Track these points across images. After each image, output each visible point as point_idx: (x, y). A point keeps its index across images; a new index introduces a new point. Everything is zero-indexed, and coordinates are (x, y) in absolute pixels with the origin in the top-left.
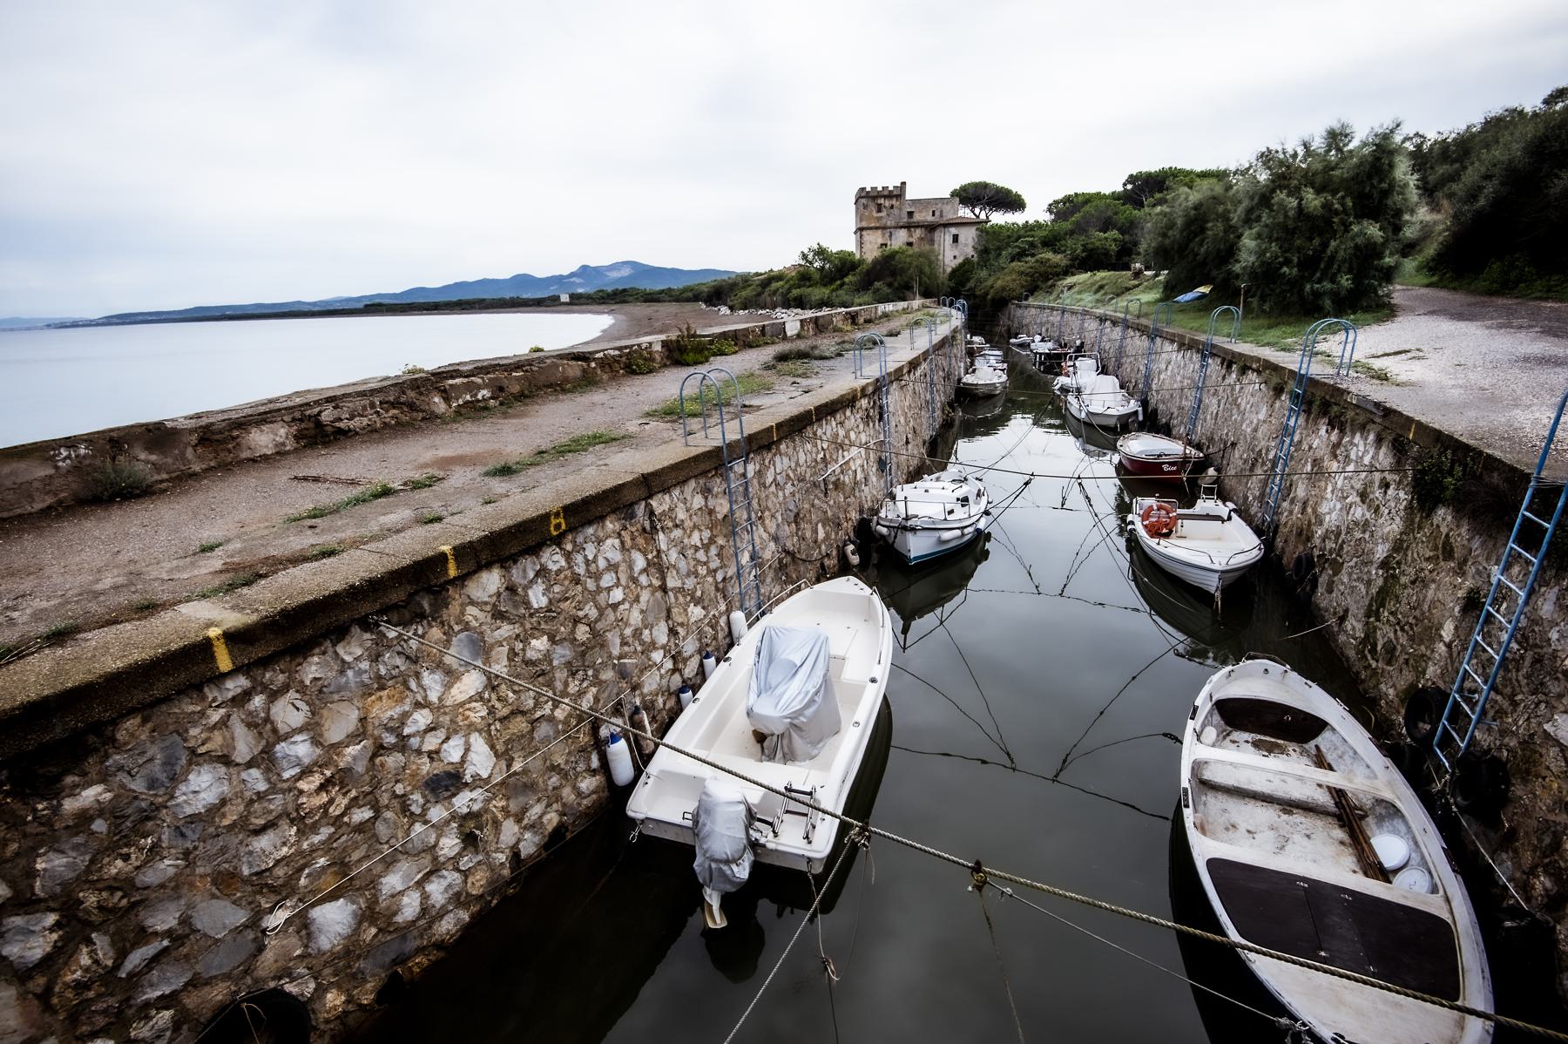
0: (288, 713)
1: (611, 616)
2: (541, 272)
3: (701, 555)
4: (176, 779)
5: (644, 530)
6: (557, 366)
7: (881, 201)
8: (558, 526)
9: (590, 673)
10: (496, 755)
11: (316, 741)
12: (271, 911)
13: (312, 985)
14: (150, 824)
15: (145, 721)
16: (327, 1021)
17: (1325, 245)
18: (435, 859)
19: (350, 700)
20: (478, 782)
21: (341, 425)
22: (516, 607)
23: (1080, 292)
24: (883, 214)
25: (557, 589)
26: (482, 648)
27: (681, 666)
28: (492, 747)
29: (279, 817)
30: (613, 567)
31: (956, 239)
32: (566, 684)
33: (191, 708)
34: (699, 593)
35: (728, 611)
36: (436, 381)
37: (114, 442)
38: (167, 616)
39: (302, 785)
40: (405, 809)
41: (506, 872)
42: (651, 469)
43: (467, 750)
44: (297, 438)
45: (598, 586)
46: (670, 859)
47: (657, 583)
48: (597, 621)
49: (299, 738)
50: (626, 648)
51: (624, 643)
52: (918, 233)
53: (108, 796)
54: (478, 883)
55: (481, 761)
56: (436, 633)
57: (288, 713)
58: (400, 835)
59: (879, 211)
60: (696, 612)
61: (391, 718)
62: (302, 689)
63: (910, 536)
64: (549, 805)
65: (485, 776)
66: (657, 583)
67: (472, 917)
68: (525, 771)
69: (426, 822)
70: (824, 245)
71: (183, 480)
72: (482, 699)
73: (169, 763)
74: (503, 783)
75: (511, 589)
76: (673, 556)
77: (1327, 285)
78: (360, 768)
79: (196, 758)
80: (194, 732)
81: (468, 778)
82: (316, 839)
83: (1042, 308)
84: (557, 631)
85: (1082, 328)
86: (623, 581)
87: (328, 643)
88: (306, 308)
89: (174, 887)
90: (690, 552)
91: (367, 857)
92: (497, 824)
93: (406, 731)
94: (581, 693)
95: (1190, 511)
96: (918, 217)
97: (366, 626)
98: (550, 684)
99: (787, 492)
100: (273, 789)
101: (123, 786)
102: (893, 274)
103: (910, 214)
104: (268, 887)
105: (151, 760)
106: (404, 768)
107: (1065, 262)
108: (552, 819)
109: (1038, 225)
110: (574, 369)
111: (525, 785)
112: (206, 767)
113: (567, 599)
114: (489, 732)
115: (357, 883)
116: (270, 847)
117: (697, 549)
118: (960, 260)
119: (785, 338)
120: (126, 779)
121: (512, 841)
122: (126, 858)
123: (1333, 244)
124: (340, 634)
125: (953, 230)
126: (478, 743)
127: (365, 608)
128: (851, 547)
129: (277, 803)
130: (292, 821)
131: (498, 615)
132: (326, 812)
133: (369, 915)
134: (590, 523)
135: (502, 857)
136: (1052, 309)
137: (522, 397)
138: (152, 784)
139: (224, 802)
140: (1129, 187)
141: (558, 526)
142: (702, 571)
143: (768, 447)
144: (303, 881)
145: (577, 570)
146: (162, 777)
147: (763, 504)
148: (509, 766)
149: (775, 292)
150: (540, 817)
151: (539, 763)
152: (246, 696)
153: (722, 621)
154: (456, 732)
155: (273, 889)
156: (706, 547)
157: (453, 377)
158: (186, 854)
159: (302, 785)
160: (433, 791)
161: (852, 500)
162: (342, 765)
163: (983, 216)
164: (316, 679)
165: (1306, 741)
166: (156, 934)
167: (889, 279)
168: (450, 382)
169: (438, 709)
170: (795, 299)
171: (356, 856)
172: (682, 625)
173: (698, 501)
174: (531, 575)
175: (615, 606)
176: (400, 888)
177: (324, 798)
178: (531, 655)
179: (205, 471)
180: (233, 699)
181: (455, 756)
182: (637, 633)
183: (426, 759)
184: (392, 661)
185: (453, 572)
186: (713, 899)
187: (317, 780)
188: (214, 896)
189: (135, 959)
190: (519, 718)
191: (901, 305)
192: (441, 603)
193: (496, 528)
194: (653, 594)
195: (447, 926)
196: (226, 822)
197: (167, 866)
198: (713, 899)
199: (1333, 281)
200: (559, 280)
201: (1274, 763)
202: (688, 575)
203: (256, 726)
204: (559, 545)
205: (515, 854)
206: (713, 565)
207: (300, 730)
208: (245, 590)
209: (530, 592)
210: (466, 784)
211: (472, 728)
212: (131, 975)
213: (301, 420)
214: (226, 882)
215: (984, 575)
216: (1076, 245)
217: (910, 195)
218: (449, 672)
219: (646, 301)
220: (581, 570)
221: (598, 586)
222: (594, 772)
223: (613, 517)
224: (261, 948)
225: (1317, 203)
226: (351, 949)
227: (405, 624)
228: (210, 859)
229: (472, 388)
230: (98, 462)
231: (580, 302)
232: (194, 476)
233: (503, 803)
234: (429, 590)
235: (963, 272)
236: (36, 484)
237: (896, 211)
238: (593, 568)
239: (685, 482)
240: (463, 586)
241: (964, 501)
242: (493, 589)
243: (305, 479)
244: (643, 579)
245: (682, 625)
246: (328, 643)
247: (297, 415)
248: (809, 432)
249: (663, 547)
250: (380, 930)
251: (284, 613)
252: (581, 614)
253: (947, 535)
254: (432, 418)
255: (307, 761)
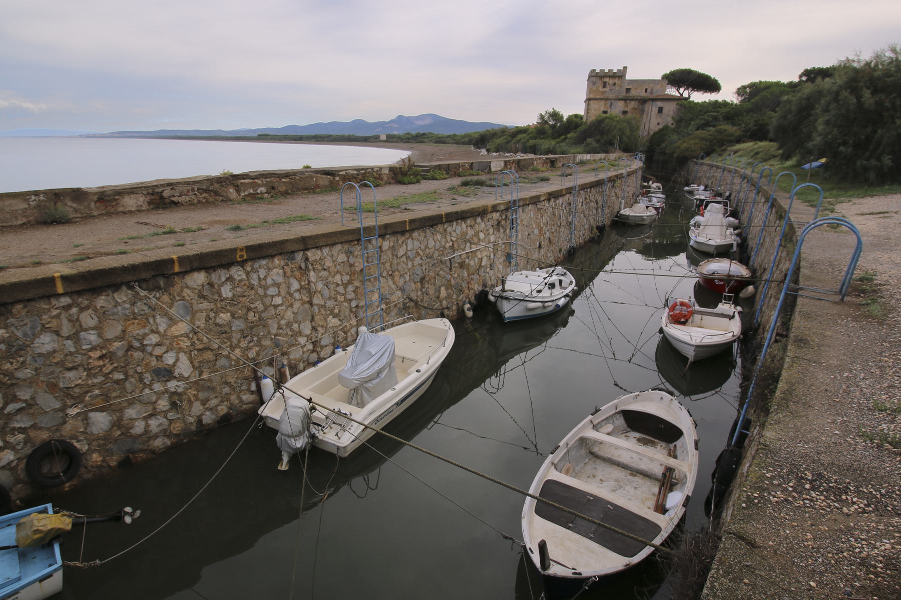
0: (88, 319)
1: (272, 311)
2: (371, 119)
3: (341, 289)
4: (36, 336)
5: (300, 268)
6: (312, 177)
7: (607, 80)
8: (241, 256)
9: (255, 339)
10: (193, 366)
11: (100, 335)
12: (71, 406)
13: (86, 447)
14: (22, 352)
15: (25, 307)
16: (92, 467)
17: (875, 132)
18: (155, 409)
19: (118, 320)
20: (181, 378)
21: (174, 199)
22: (213, 294)
23: (741, 156)
24: (607, 89)
25: (239, 289)
26: (192, 313)
27: (319, 349)
28: (191, 362)
29: (79, 365)
30: (278, 285)
31: (660, 110)
32: (239, 341)
33: (45, 306)
34: (336, 311)
35: (358, 326)
36: (232, 180)
37: (57, 195)
38: (43, 267)
39: (91, 354)
40: (141, 380)
41: (193, 428)
42: (308, 234)
43: (177, 360)
44: (149, 203)
45: (265, 293)
46: (267, 433)
47: (306, 299)
48: (262, 312)
49: (92, 332)
50: (281, 331)
51: (279, 328)
52: (633, 104)
53: (7, 335)
54: (177, 428)
55: (184, 367)
56: (166, 298)
57: (88, 319)
58: (137, 391)
59: (604, 86)
60: (333, 322)
61: (138, 334)
62: (96, 310)
63: (505, 302)
64: (222, 401)
65: (186, 376)
66: (306, 299)
67: (172, 444)
68: (209, 380)
69: (151, 389)
70: (557, 110)
71: (88, 217)
72: (188, 337)
73: (33, 328)
74: (196, 382)
75: (211, 285)
76: (320, 286)
77: (874, 162)
78: (120, 353)
79: (45, 329)
80: (44, 317)
81: (176, 374)
82: (95, 381)
83: (711, 166)
84: (237, 312)
85: (732, 183)
86: (283, 293)
87: (110, 291)
88: (224, 135)
89: (30, 382)
90: (332, 286)
91: (119, 397)
92: (190, 402)
93: (145, 342)
94: (248, 349)
95: (715, 311)
96: (633, 93)
97: (131, 288)
98: (229, 339)
99: (416, 263)
100: (77, 352)
101: (13, 333)
102: (602, 133)
103: (628, 90)
104: (69, 395)
105: (26, 324)
106: (143, 360)
107: (739, 133)
108: (223, 409)
109: (725, 104)
110: (325, 180)
111: (209, 387)
112: (48, 334)
113: (244, 296)
114: (190, 355)
115: (113, 408)
116: (73, 378)
117: (338, 285)
118: (661, 127)
119: (490, 172)
120: (15, 331)
121: (199, 413)
122: (12, 363)
123: (879, 131)
124: (116, 287)
125: (660, 104)
126: (183, 358)
127: (129, 278)
128: (468, 306)
129: (79, 359)
130: (85, 369)
131: (202, 296)
132: (101, 370)
133: (117, 424)
134: (264, 258)
135: (192, 420)
136: (718, 167)
137: (286, 194)
138: (25, 335)
139: (54, 351)
140: (804, 78)
141: (241, 256)
142: (340, 298)
143: (403, 233)
144: (87, 398)
145: (253, 282)
146: (29, 333)
147: (395, 267)
148: (200, 375)
149: (519, 141)
150: (216, 406)
151: (218, 378)
152: (67, 308)
153: (353, 331)
154: (172, 350)
155: (73, 397)
156: (345, 286)
157: (244, 179)
158: (36, 369)
159: (91, 354)
160: (157, 375)
161: (476, 277)
162: (111, 350)
163: (686, 95)
164: (102, 307)
165: (671, 442)
166: (20, 400)
167: (598, 137)
168: (243, 181)
169: (163, 336)
170: (531, 147)
171: (114, 394)
172: (322, 326)
173: (342, 258)
174: (223, 279)
175: (276, 307)
176: (134, 417)
177: (101, 363)
178: (218, 321)
179: (99, 215)
180: (63, 307)
181: (171, 361)
182: (289, 325)
183: (154, 359)
184: (140, 307)
185: (177, 269)
186: (285, 459)
187: (98, 354)
188: (46, 392)
189: (12, 407)
190: (209, 352)
191: (602, 156)
192: (170, 284)
193: (204, 251)
194: (303, 304)
195: (159, 443)
196: (54, 361)
197: (27, 373)
198: (285, 459)
199: (878, 159)
200: (382, 124)
201: (648, 450)
202: (330, 298)
203: (73, 321)
204: (242, 267)
205: (199, 421)
206: (349, 297)
207: (93, 329)
208: (80, 263)
209: (222, 289)
210: (175, 377)
211: (180, 350)
212: (9, 414)
213: (152, 194)
214: (52, 387)
215: (562, 337)
216: (750, 121)
217: (629, 76)
218: (171, 319)
219: (436, 142)
220: (255, 282)
221: (265, 293)
222: (252, 392)
223: (280, 257)
224: (65, 422)
225: (872, 101)
226: (107, 437)
227: (150, 290)
228: (47, 375)
229: (255, 186)
230: (47, 204)
231: (393, 141)
232: (93, 216)
233: (195, 392)
234: (163, 275)
235: (660, 136)
236: (19, 212)
237: (617, 88)
238: (263, 283)
239: (334, 244)
240: (183, 278)
241: (552, 286)
242: (200, 282)
243: (142, 223)
244: (297, 295)
245: (322, 326)
246: (110, 291)
247: (150, 191)
248: (440, 228)
249: (313, 279)
250: (122, 433)
251: (89, 272)
252: (252, 306)
253: (532, 305)
254: (227, 200)
255: (94, 344)
